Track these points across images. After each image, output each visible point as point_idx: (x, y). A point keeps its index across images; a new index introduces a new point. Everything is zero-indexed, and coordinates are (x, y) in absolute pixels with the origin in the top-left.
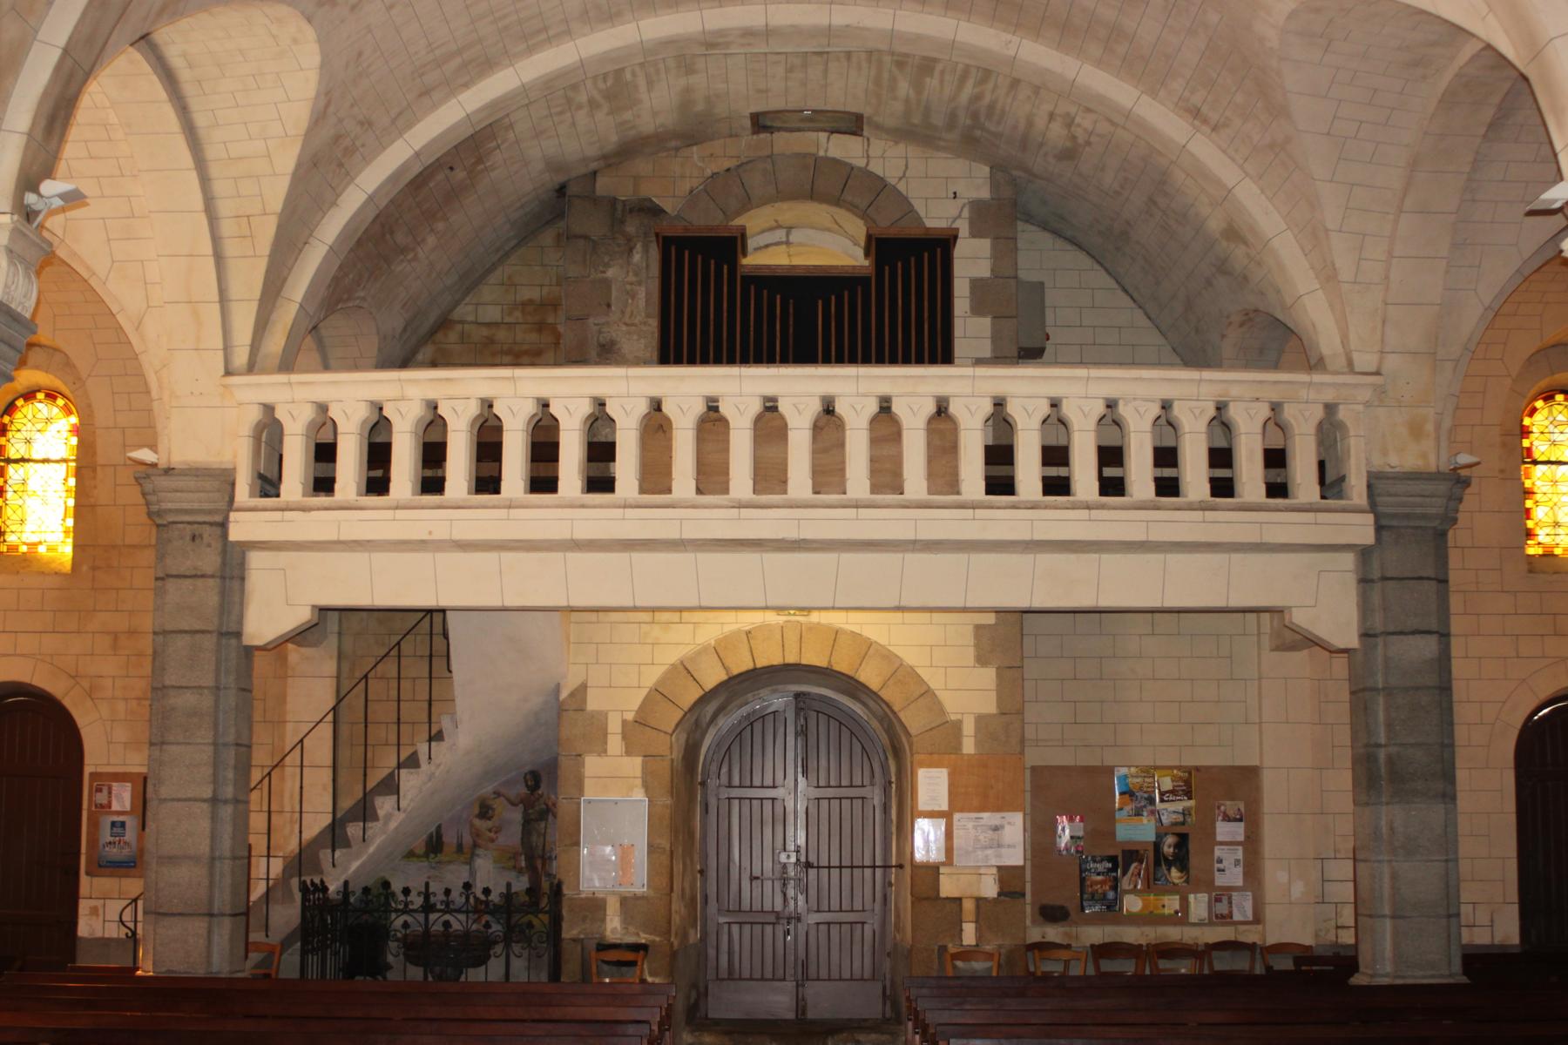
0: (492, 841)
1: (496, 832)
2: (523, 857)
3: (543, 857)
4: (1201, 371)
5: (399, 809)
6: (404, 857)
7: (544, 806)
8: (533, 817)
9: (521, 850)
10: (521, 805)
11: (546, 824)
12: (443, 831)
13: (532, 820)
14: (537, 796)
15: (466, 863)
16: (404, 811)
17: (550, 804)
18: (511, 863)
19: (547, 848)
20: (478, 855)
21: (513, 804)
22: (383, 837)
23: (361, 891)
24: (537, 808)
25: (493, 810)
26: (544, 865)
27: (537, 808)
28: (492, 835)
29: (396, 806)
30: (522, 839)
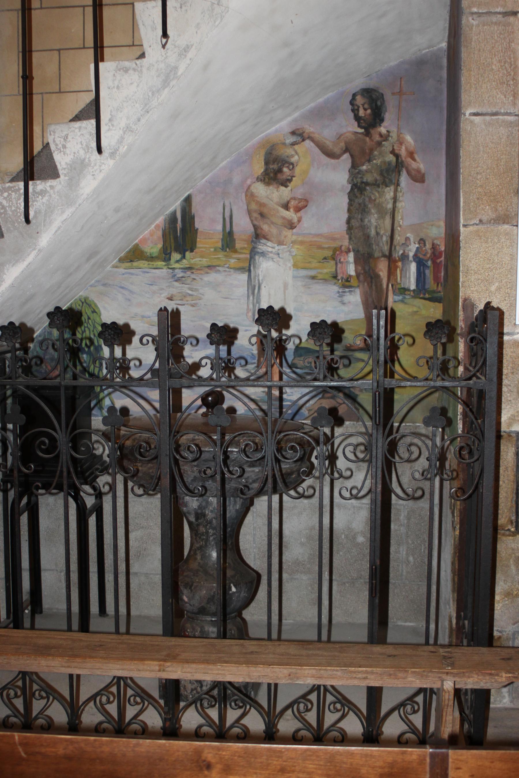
0: (291, 226)
1: (298, 210)
2: (351, 257)
3: (389, 257)
4: (461, 107)
5: (99, 150)
6: (121, 260)
7: (391, 158)
8: (369, 178)
9: (346, 243)
10: (346, 156)
11: (396, 191)
12: (196, 208)
13: (367, 184)
14: (377, 138)
15: (241, 269)
16: (112, 155)
17: (403, 152)
18: (329, 268)
19: (398, 238)
20: (263, 254)
21: (330, 154)
22: (68, 212)
23: (47, 321)
24: (377, 161)
25: (292, 166)
26: (391, 272)
27: (377, 161)
28: (290, 215)
29: (94, 145)
30: (348, 222)
